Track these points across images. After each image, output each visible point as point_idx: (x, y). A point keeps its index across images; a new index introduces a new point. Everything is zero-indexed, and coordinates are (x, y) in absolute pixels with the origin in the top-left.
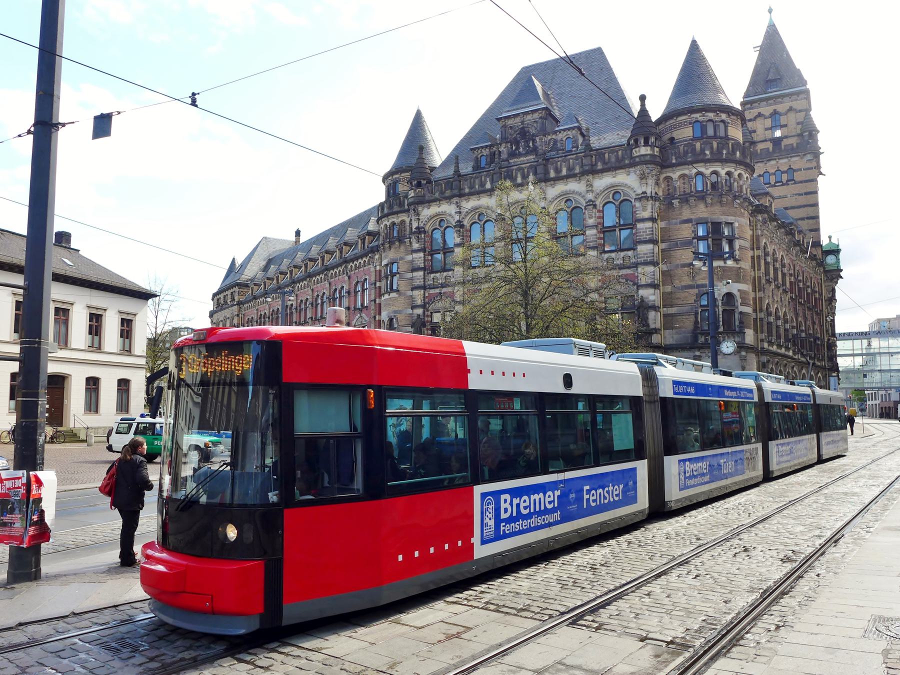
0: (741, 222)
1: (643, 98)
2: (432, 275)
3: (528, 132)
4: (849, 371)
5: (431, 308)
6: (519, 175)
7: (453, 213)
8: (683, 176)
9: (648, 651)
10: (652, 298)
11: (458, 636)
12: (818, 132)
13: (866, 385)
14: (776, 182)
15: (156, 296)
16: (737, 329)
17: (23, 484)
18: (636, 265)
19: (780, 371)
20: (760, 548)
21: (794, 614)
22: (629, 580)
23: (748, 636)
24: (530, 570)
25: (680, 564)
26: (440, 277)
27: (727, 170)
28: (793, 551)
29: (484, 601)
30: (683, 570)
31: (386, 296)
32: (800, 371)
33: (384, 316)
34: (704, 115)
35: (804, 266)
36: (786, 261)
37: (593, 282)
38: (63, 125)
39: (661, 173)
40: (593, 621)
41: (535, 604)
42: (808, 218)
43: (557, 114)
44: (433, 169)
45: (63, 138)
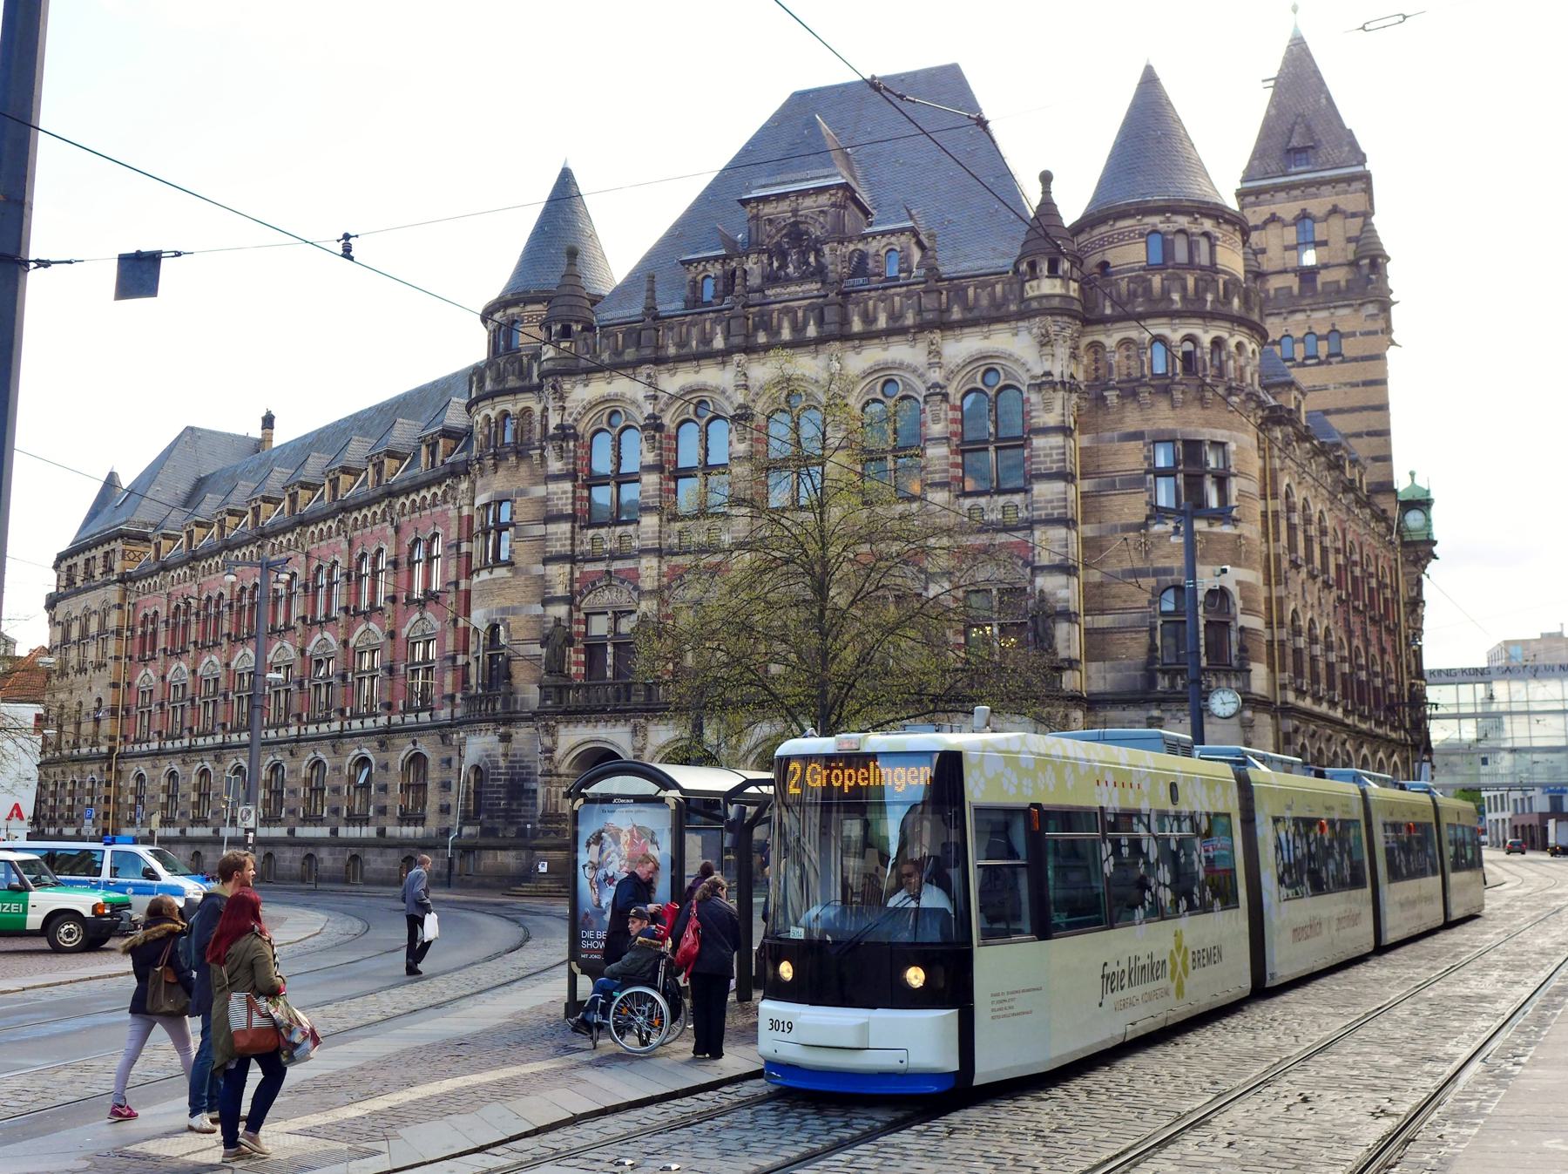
0: (1241, 442)
16: (1235, 663)
27: (1214, 333)
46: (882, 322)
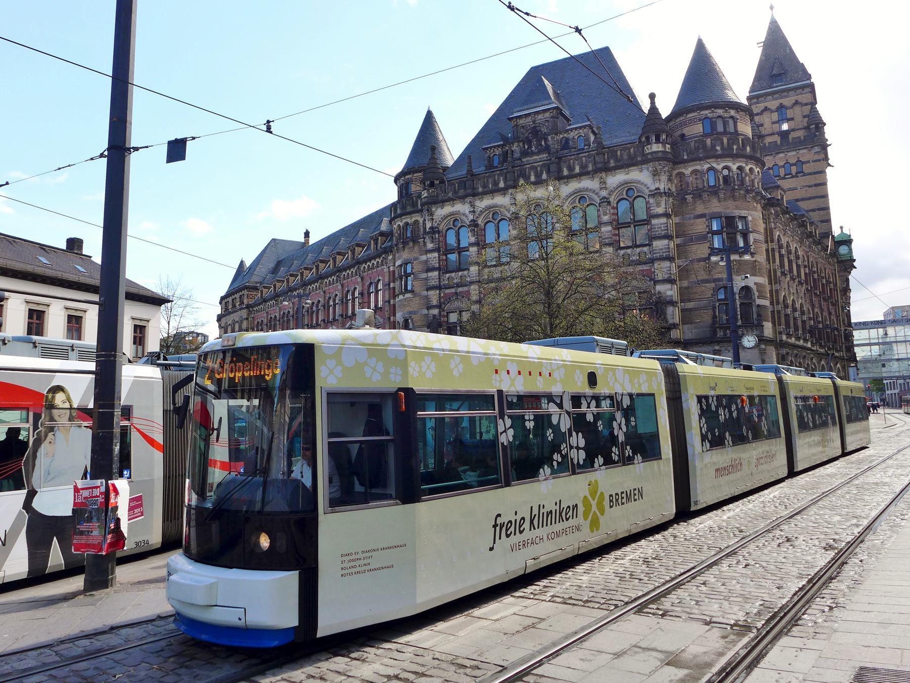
0: (754, 216)
1: (652, 97)
2: (447, 275)
3: (540, 131)
4: (866, 361)
5: (447, 307)
6: (532, 174)
7: (467, 212)
8: (695, 172)
9: (716, 633)
10: (669, 293)
11: (533, 626)
12: (825, 124)
13: (885, 375)
14: (786, 175)
15: (169, 301)
16: (755, 322)
17: (101, 493)
18: (652, 261)
19: (800, 363)
20: (801, 538)
21: (844, 596)
22: (682, 571)
23: (805, 616)
24: (586, 566)
25: (727, 555)
26: (456, 277)
27: (738, 164)
28: (834, 540)
29: (549, 594)
30: (733, 560)
31: (401, 297)
32: (819, 363)
33: (399, 316)
34: (713, 112)
35: (816, 257)
36: (800, 253)
37: (610, 279)
38: (136, 149)
39: (673, 169)
40: (658, 609)
41: (598, 595)
42: (819, 209)
43: (567, 113)
44: (445, 169)
45: (136, 163)
46: (577, 170)
